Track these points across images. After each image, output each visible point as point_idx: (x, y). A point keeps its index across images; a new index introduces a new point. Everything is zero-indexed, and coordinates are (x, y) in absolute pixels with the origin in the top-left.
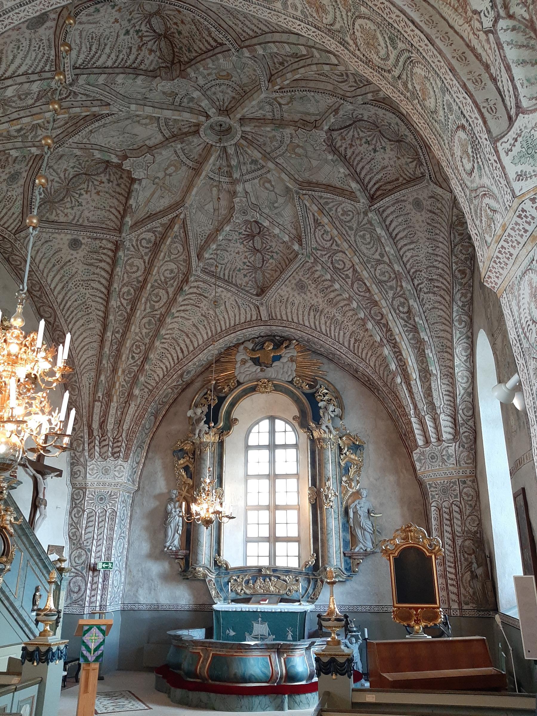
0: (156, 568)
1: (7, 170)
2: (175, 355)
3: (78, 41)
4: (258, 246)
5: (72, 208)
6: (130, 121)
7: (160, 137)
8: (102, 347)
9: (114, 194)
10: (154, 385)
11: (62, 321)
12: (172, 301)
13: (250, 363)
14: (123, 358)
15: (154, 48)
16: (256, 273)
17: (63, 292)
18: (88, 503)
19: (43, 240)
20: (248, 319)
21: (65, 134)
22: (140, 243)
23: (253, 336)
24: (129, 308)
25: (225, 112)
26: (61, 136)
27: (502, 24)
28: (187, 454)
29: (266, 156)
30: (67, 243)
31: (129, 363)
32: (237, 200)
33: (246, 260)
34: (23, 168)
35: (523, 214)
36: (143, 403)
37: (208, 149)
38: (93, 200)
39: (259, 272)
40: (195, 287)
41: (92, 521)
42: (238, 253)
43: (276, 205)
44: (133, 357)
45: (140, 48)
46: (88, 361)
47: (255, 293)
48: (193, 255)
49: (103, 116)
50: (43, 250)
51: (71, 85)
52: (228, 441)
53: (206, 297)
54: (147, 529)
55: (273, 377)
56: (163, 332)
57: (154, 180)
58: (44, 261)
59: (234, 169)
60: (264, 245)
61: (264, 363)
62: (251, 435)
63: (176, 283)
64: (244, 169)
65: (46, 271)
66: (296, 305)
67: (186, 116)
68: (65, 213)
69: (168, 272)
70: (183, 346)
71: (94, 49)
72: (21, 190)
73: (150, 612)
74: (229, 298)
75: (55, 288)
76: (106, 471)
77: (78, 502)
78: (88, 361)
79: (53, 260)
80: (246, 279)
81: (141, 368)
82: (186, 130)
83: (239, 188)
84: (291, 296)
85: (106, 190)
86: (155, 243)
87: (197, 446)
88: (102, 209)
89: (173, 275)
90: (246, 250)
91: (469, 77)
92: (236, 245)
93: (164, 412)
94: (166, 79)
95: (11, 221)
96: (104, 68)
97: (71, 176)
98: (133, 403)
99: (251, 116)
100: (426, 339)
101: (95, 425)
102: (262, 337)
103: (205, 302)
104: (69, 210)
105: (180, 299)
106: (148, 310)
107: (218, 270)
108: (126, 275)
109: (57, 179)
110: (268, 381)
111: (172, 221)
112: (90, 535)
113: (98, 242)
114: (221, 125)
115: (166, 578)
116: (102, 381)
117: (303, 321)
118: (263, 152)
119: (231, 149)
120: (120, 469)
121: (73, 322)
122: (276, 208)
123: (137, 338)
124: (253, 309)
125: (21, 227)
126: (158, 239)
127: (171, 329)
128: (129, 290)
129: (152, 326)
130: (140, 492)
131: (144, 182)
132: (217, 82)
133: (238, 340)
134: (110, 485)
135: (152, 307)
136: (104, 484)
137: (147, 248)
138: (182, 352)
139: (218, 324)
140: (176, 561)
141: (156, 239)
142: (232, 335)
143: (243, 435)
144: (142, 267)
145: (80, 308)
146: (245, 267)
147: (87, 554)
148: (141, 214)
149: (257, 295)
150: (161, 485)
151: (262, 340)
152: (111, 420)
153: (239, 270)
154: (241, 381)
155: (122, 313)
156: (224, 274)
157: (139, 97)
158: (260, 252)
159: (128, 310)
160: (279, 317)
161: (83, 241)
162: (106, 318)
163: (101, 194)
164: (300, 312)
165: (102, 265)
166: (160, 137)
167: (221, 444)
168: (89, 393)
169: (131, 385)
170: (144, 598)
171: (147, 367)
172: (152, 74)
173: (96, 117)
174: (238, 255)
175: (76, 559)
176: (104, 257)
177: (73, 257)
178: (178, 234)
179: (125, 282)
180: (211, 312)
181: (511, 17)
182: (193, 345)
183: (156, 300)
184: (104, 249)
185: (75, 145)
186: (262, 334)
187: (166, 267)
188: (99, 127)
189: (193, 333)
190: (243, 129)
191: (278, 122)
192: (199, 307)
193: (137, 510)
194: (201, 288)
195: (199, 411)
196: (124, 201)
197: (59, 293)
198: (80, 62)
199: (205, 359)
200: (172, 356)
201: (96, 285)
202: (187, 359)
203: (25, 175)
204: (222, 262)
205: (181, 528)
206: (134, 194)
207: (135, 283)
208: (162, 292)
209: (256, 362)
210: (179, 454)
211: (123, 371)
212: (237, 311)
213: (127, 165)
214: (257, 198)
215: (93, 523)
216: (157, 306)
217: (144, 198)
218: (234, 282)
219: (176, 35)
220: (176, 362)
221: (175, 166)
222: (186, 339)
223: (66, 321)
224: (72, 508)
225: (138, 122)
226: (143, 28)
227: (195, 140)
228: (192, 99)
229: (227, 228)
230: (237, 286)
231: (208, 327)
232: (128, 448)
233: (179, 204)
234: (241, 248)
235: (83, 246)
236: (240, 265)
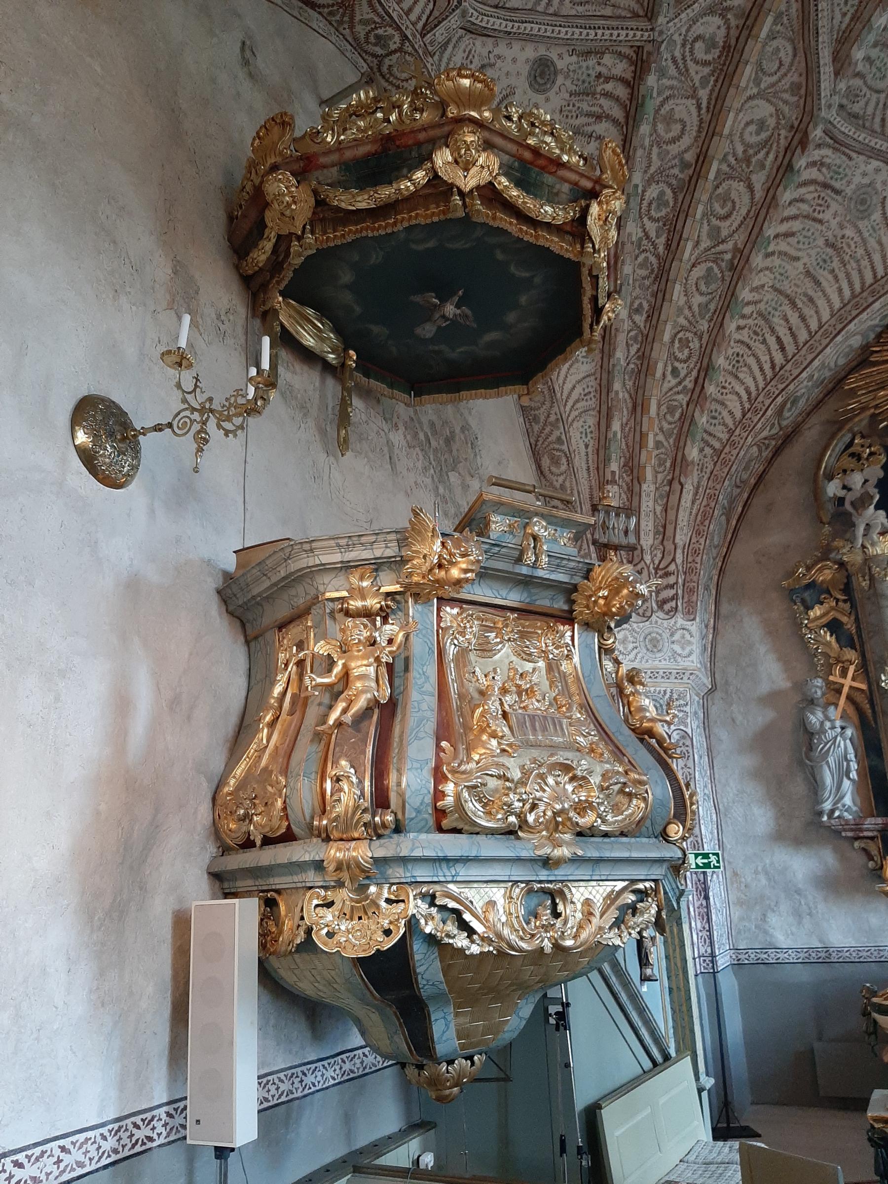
0: (802, 865)
2: (765, 358)
10: (724, 436)
14: (659, 374)
28: (828, 592)
30: (525, 70)
31: (666, 386)
36: (704, 482)
44: (675, 372)
46: (578, 390)
48: (825, 56)
54: (756, 774)
56: (745, 294)
63: (771, 156)
69: (752, 128)
70: (783, 332)
73: (808, 966)
78: (578, 390)
86: (726, 47)
89: (764, 135)
93: (740, 509)
100: (496, 689)
103: (834, 206)
108: (655, 150)
115: (833, 886)
116: (615, 434)
120: (683, 637)
123: (682, 321)
125: (436, 13)
126: (734, 33)
128: (662, 193)
129: (713, 287)
130: (718, 694)
134: (667, 675)
135: (715, 232)
137: (706, 63)
138: (783, 349)
139: (865, 263)
140: (857, 844)
141: (727, 36)
144: (692, 121)
150: (771, 672)
159: (661, 249)
168: (588, 469)
170: (787, 935)
176: (606, 103)
179: (653, 169)
180: (849, 232)
182: (807, 327)
183: (722, 212)
184: (607, 80)
189: (806, 295)
192: (820, 222)
193: (722, 734)
194: (829, 167)
199: (832, 365)
202: (796, 364)
205: (854, 766)
207: (676, 171)
208: (737, 188)
210: (807, 595)
216: (726, 228)
220: (769, 373)
222: (790, 313)
231: (841, 275)
235: (560, 80)
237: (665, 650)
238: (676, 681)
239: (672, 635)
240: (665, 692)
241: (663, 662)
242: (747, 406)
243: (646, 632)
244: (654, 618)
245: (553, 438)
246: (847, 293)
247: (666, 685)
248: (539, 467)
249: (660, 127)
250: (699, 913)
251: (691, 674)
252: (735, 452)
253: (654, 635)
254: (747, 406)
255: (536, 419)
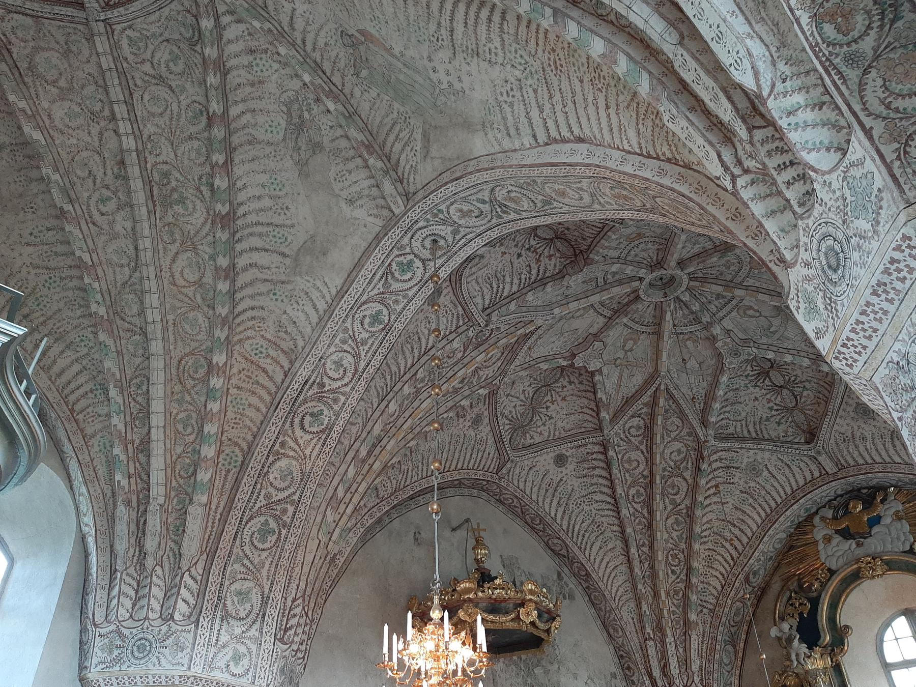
1: (468, 418)
2: (726, 555)
3: (478, 288)
4: (779, 381)
5: (544, 424)
6: (564, 320)
7: (602, 320)
8: (631, 569)
9: (579, 394)
10: (714, 601)
11: (576, 549)
12: (694, 488)
13: (837, 539)
15: (551, 253)
16: (791, 414)
17: (567, 517)
19: (527, 468)
20: (809, 478)
21: (505, 363)
22: (629, 433)
23: (827, 499)
24: (645, 512)
25: (658, 266)
26: (502, 367)
27: (740, 182)
29: (729, 285)
31: (670, 580)
32: (719, 344)
33: (771, 404)
34: (482, 408)
36: (708, 629)
37: (660, 308)
38: (562, 408)
39: (796, 413)
40: (716, 461)
42: (756, 399)
43: (772, 329)
44: (673, 572)
45: (538, 260)
46: (621, 590)
47: (802, 441)
49: (532, 333)
50: (530, 479)
51: (486, 326)
52: (847, 662)
53: (737, 468)
55: (879, 550)
56: (698, 529)
57: (615, 363)
58: (535, 490)
59: (699, 314)
60: (787, 378)
61: (858, 533)
62: (885, 644)
63: (690, 464)
64: (713, 308)
65: (541, 500)
66: (869, 438)
67: (616, 290)
68: (539, 432)
69: (675, 453)
71: (495, 285)
72: (489, 428)
74: (769, 459)
75: (556, 515)
79: (544, 486)
80: (782, 426)
81: (689, 585)
82: (626, 300)
83: (717, 330)
84: (856, 428)
85: (571, 392)
86: (646, 427)
87: (802, 677)
88: (574, 414)
89: (682, 455)
90: (765, 392)
91: (747, 233)
92: (749, 391)
93: (744, 637)
94: (575, 273)
95: (489, 462)
96: (511, 297)
97: (531, 395)
98: (694, 633)
99: (690, 255)
101: (656, 673)
102: (842, 496)
103: (738, 475)
104: (542, 428)
105: (703, 482)
106: (670, 507)
107: (739, 430)
108: (627, 475)
109: (520, 403)
110: (874, 559)
111: (655, 397)
113: (582, 449)
114: (661, 279)
116: (645, 612)
117: (890, 457)
118: (723, 283)
119: (684, 296)
121: (588, 548)
122: (774, 333)
123: (670, 545)
124: (809, 462)
126: (648, 422)
127: (708, 522)
128: (638, 491)
129: (681, 526)
131: (605, 370)
132: (632, 245)
133: (807, 510)
135: (673, 502)
142: (795, 507)
143: (872, 648)
145: (590, 529)
146: (774, 413)
148: (617, 402)
149: (807, 442)
151: (842, 500)
152: (673, 662)
153: (768, 419)
154: (834, 568)
155: (640, 521)
156: (749, 431)
157: (559, 298)
158: (785, 388)
159: (646, 515)
160: (852, 463)
161: (568, 454)
162: (623, 532)
163: (567, 399)
164: (880, 447)
165: (597, 472)
166: (602, 320)
167: (837, 668)
169: (684, 608)
171: (694, 580)
172: (560, 275)
173: (527, 336)
174: (756, 402)
177: (563, 474)
178: (668, 407)
180: (752, 484)
181: (747, 171)
183: (672, 492)
184: (592, 454)
185: (518, 369)
186: (839, 492)
187: (670, 450)
188: (536, 341)
190: (686, 272)
191: (722, 247)
192: (733, 483)
195: (785, 626)
196: (593, 397)
197: (562, 519)
198: (487, 302)
200: (723, 556)
201: (599, 497)
203: (486, 413)
204: (739, 418)
206: (598, 386)
207: (642, 480)
208: (678, 481)
209: (846, 534)
211: (668, 594)
212: (787, 471)
213: (578, 362)
214: (745, 331)
217: (612, 386)
218: (766, 436)
219: (566, 232)
221: (631, 339)
222: (733, 529)
223: (580, 548)
225: (573, 317)
226: (533, 243)
227: (640, 306)
228: (614, 274)
229: (724, 379)
230: (773, 440)
231: (756, 506)
233: (655, 375)
234: (758, 392)
235: (570, 459)
236: (764, 413)
242: (723, 582)
245: (611, 618)
246: (763, 514)
248: (609, 634)
249: (626, 465)
252: (721, 610)
254: (723, 582)
255: (600, 609)
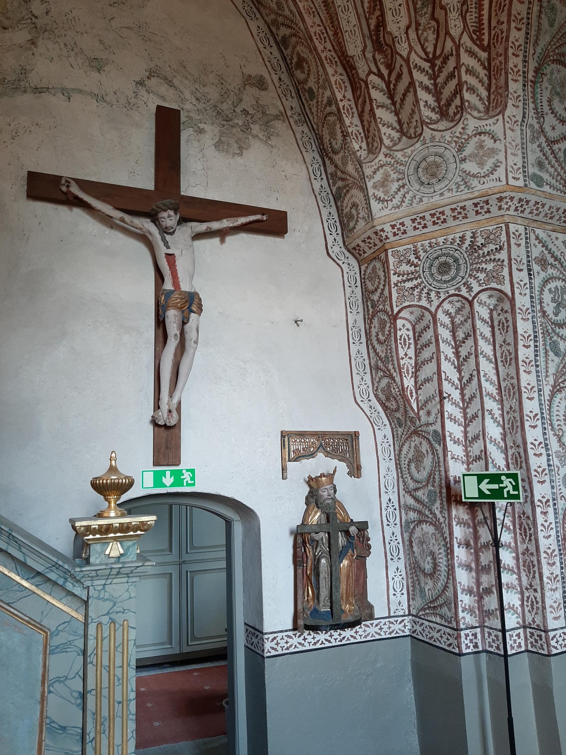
18: (400, 290)
35: (515, 645)
41: (427, 345)
76: (432, 172)
77: (375, 297)
101: (354, 46)
112: (430, 389)
120: (481, 146)
134: (460, 213)
136: (438, 217)
147: (434, 451)
175: (413, 466)
215: (433, 348)
224: (368, 319)
232: (494, 71)
237: (450, 176)
238: (479, 217)
239: (460, 149)
240: (463, 239)
241: (447, 194)
243: (418, 159)
244: (427, 133)
247: (464, 228)
250: (525, 562)
251: (500, 199)
253: (431, 159)
